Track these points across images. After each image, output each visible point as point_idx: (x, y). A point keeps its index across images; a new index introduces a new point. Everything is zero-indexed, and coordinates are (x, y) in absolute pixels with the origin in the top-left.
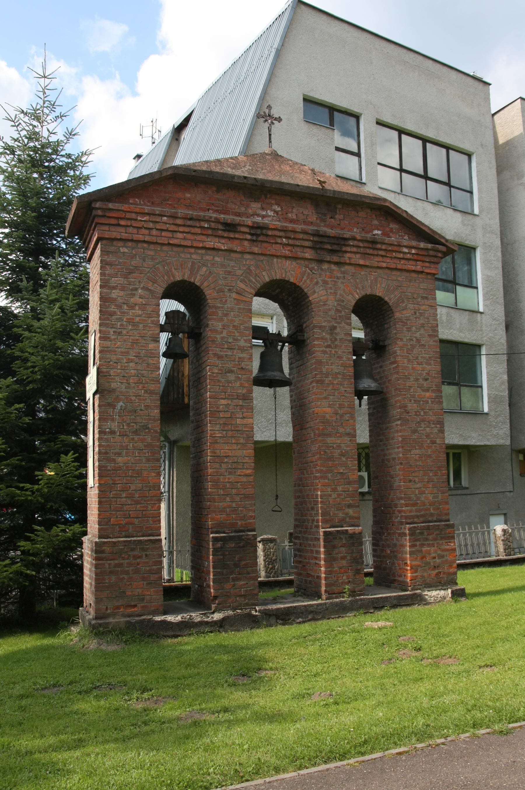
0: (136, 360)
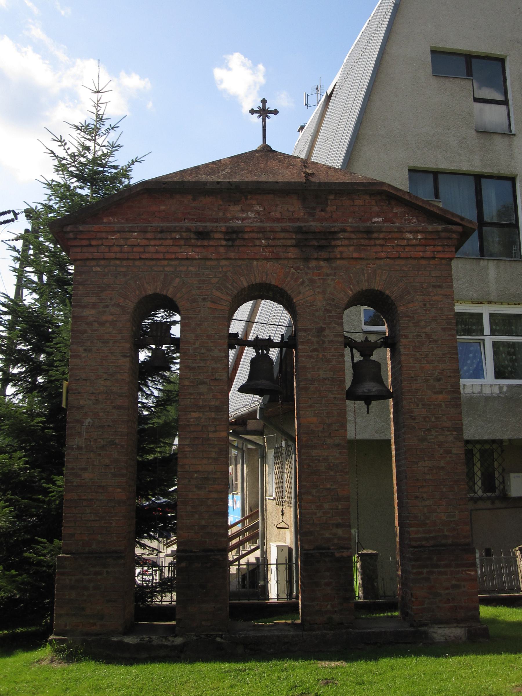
0: (105, 376)
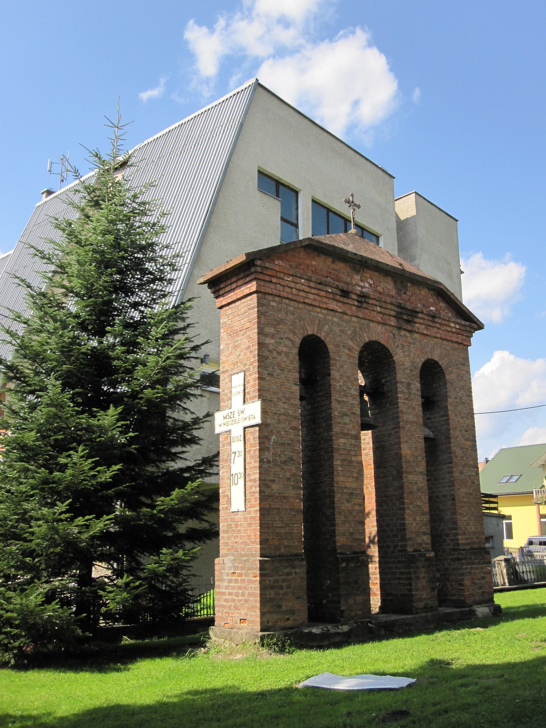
0: (284, 400)
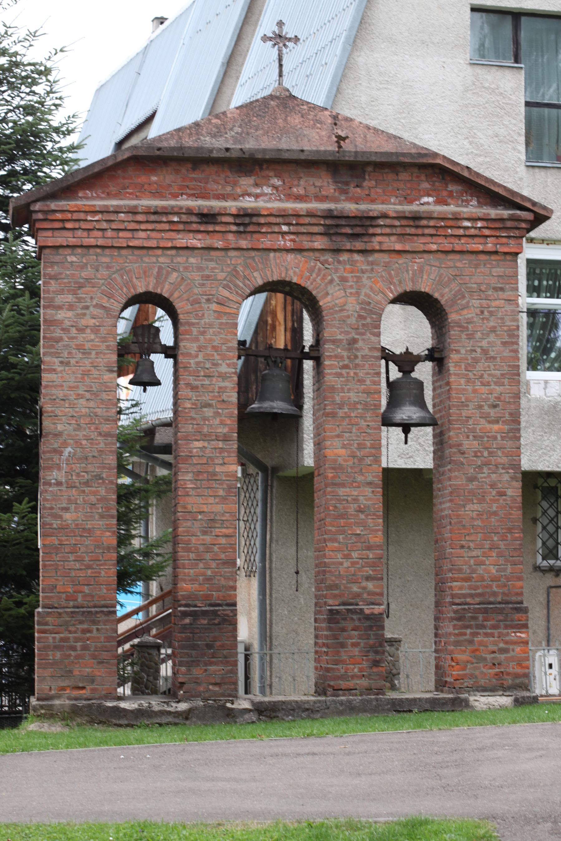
0: (88, 395)
